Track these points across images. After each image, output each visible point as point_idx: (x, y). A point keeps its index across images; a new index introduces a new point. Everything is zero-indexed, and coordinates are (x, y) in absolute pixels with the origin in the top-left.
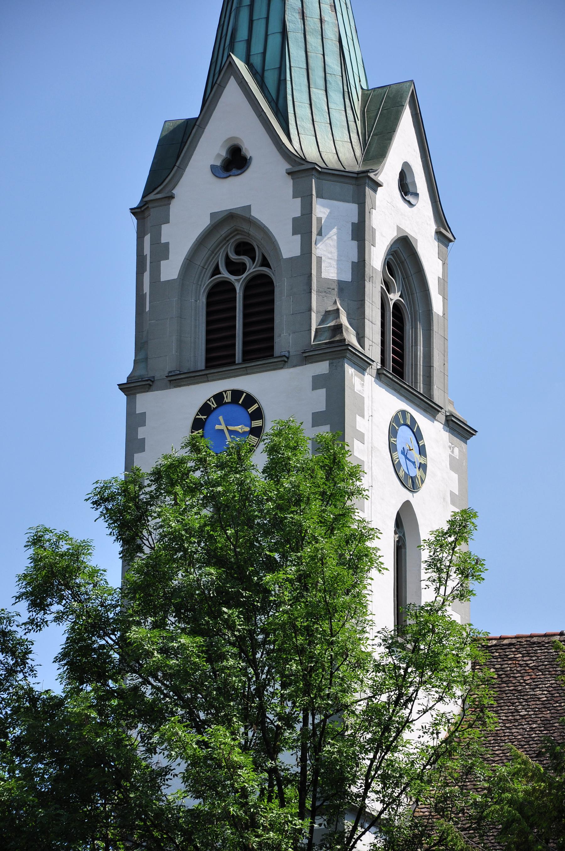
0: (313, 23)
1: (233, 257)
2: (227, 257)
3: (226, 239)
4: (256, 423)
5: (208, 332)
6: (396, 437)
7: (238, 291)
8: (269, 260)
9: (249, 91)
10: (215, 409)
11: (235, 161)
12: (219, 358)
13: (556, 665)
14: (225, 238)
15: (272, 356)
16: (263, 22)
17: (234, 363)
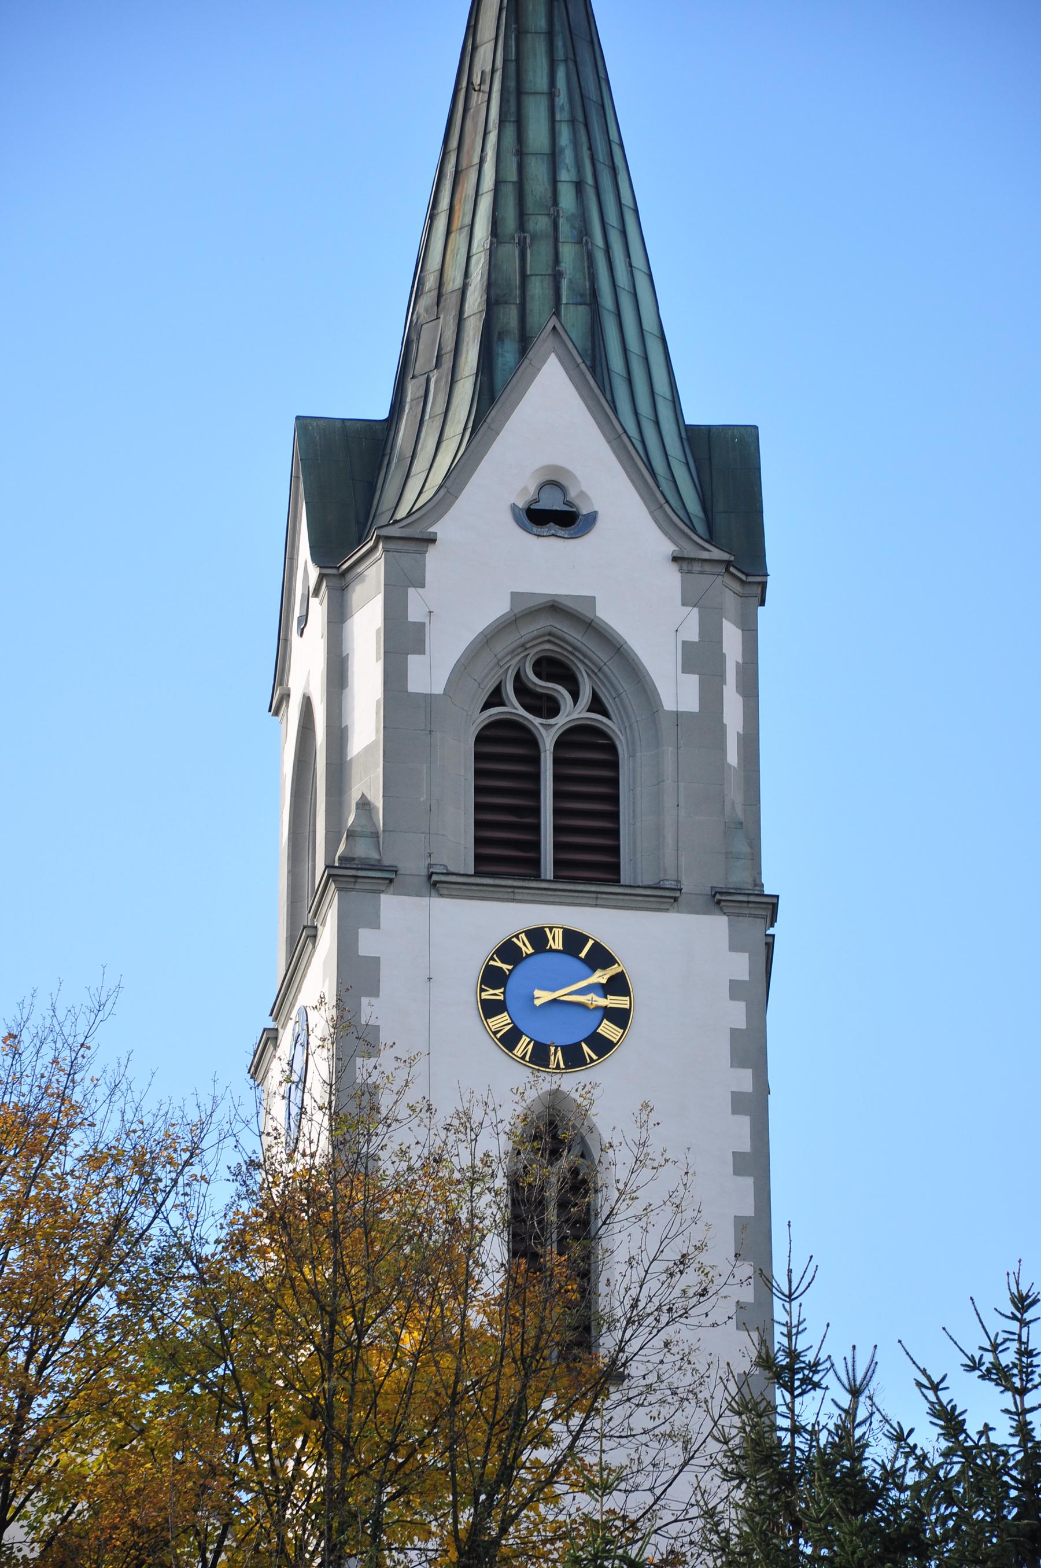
16: (466, 232)
17: (537, 877)
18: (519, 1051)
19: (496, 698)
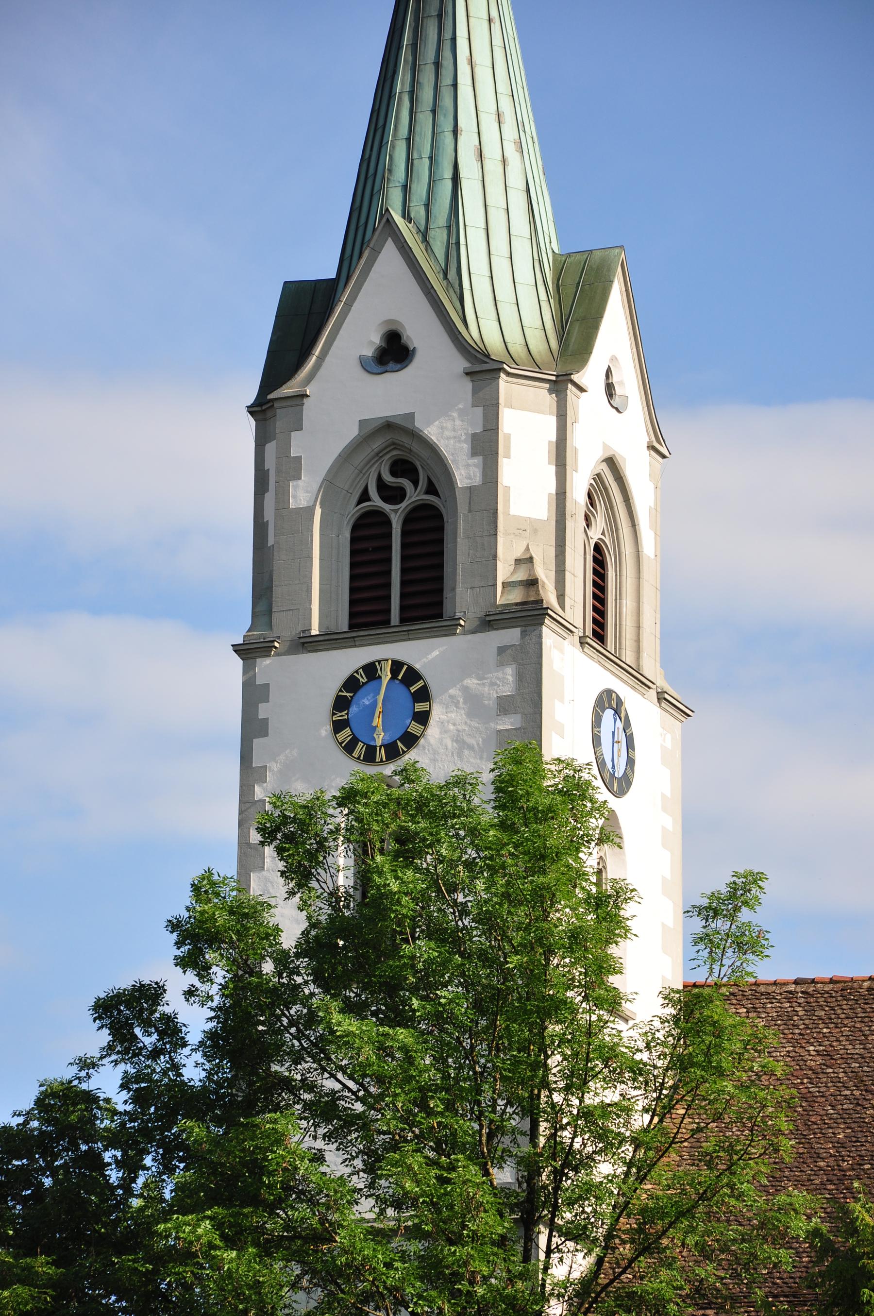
0: (493, 166)
1: (388, 478)
2: (379, 478)
3: (379, 455)
4: (420, 707)
5: (353, 578)
6: (599, 727)
7: (394, 525)
8: (437, 486)
9: (419, 269)
10: (364, 684)
11: (394, 352)
12: (366, 613)
13: (793, 1025)
14: (377, 454)
15: (440, 616)
18: (356, 754)
19: (365, 496)
